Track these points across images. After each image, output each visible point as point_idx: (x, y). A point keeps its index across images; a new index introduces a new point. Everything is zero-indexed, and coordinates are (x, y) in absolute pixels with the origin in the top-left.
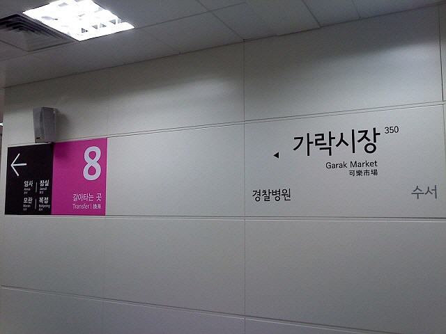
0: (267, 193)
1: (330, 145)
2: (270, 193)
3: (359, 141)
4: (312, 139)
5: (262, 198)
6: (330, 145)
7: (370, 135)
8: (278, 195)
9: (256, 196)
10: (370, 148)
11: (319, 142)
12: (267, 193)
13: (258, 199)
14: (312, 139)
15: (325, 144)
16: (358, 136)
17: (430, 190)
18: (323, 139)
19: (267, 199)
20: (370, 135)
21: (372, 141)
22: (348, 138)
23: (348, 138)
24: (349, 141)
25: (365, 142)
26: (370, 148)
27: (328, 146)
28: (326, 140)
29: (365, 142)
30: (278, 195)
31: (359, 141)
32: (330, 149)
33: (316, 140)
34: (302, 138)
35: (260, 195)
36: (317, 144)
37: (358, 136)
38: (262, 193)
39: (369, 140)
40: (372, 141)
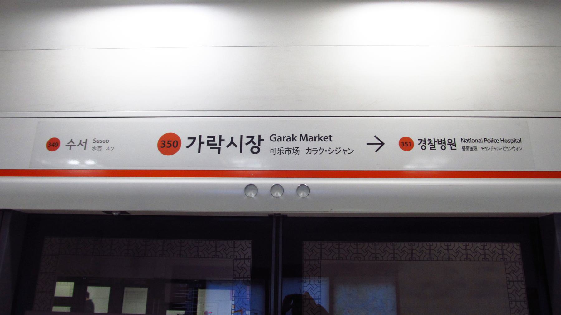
0: (433, 142)
1: (220, 145)
2: (435, 142)
3: (247, 144)
4: (205, 139)
5: (428, 147)
6: (220, 145)
7: (256, 140)
8: (444, 144)
9: (422, 144)
10: (255, 150)
11: (210, 143)
12: (433, 142)
13: (424, 148)
14: (205, 139)
15: (216, 144)
16: (246, 140)
17: (82, 143)
18: (214, 140)
19: (433, 148)
20: (256, 140)
21: (257, 145)
22: (237, 141)
23: (237, 141)
24: (238, 144)
25: (251, 145)
26: (255, 150)
27: (218, 146)
28: (217, 141)
29: (251, 145)
30: (444, 144)
31: (247, 144)
32: (219, 149)
33: (208, 141)
34: (194, 139)
35: (425, 143)
36: (208, 144)
37: (246, 140)
38: (427, 142)
39: (254, 144)
40: (257, 145)
